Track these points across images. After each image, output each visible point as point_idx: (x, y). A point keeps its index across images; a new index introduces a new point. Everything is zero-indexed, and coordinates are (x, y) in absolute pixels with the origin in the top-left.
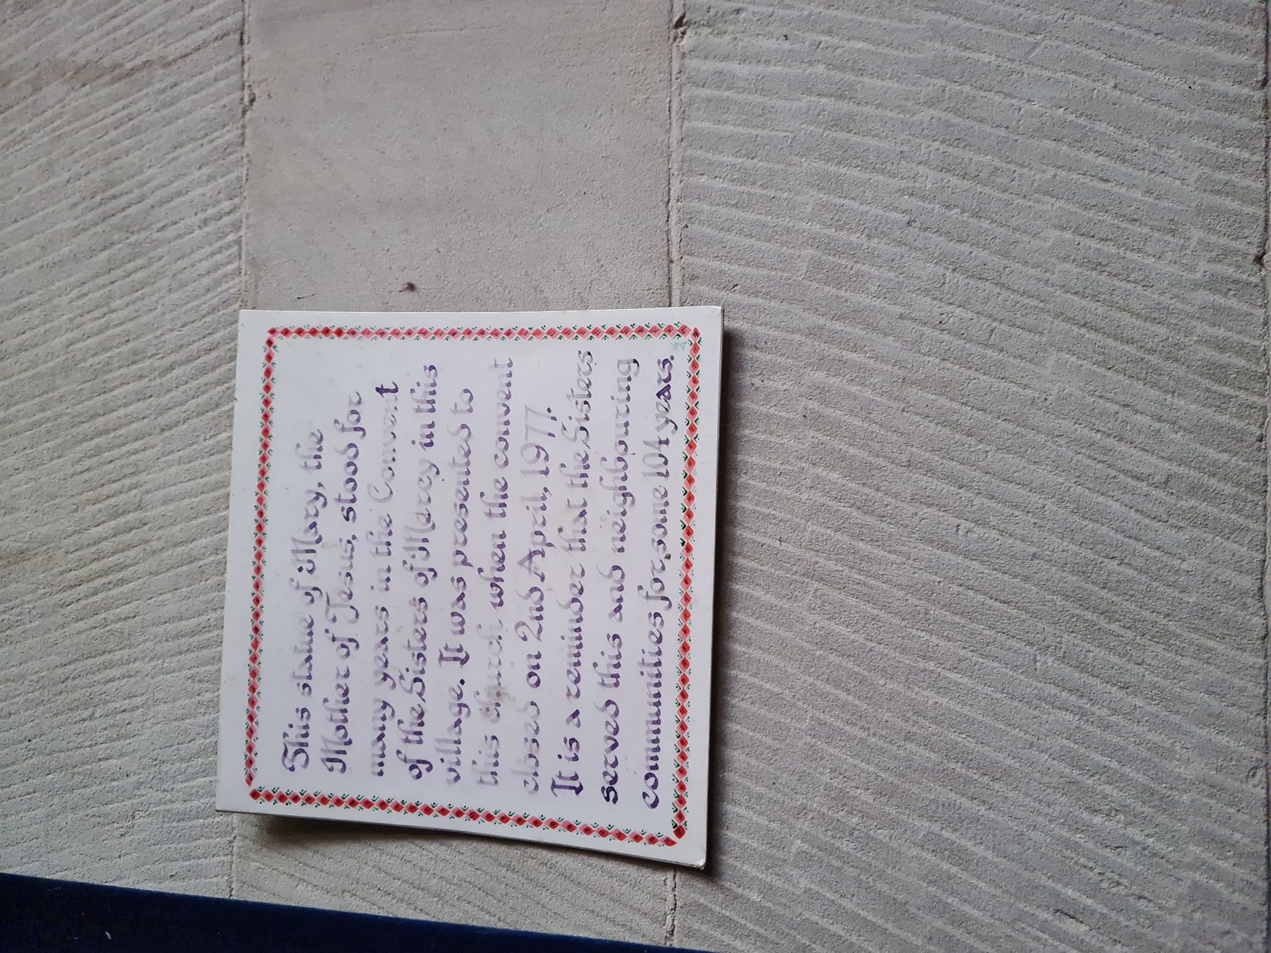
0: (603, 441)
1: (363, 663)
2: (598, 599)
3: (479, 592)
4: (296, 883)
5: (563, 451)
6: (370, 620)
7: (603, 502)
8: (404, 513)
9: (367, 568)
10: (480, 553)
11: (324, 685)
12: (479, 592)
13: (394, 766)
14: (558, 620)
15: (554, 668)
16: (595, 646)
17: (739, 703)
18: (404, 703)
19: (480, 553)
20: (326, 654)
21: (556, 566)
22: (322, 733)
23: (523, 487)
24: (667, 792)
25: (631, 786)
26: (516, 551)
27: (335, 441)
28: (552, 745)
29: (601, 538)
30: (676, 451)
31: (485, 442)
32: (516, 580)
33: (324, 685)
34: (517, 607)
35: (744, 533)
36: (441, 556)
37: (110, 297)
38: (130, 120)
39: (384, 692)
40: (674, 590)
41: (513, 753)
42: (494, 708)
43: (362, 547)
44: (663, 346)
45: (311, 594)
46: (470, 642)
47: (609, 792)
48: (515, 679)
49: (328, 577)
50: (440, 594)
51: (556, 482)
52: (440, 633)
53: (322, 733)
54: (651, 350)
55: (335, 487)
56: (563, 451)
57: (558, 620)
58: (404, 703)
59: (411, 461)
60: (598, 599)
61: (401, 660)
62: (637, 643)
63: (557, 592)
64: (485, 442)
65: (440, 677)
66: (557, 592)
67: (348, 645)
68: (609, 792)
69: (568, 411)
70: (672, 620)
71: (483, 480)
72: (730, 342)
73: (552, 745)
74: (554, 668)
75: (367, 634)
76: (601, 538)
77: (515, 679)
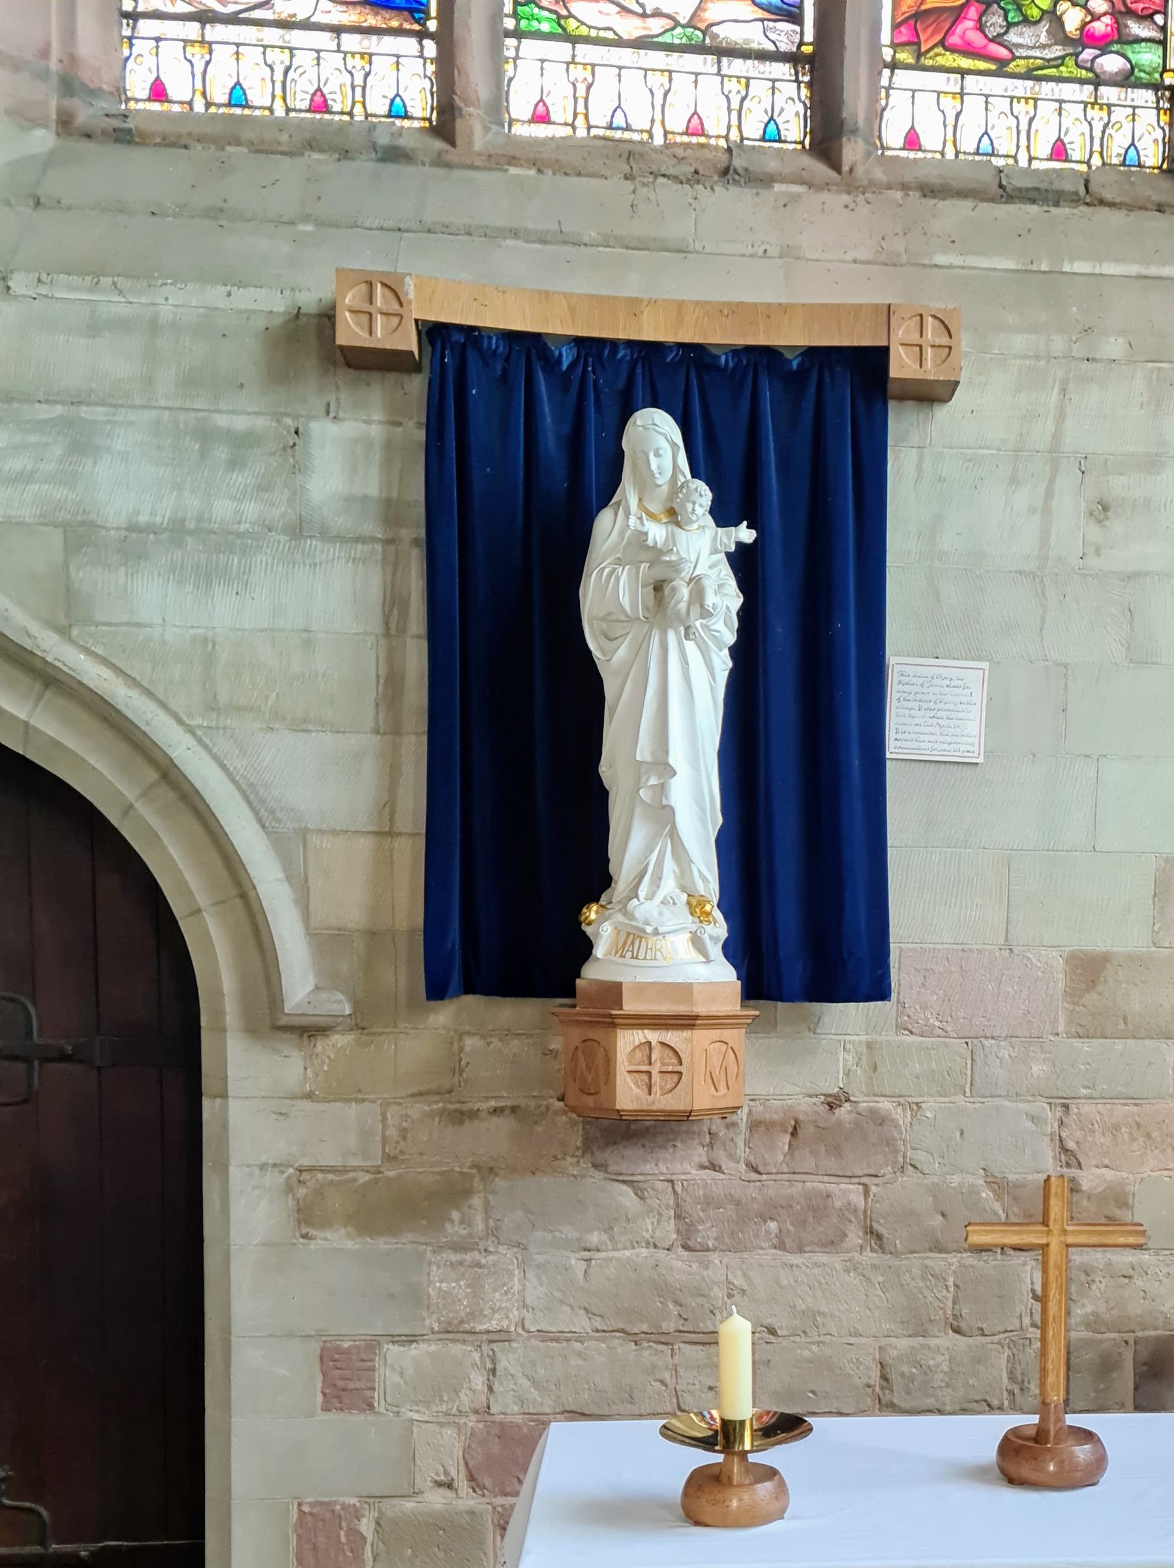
0: (960, 740)
1: (918, 689)
2: (932, 738)
3: (932, 714)
4: (54, 649)
5: (958, 731)
6: (927, 690)
7: (949, 739)
8: (946, 698)
9: (937, 690)
10: (940, 714)
11: (915, 680)
12: (932, 714)
13: (899, 694)
14: (928, 730)
15: (918, 729)
16: (922, 737)
17: (913, 764)
18: (911, 697)
19: (940, 714)
20: (920, 681)
21: (937, 730)
22: (905, 679)
23: (952, 723)
24: (897, 751)
25: (898, 744)
26: (940, 721)
27: (962, 683)
28: (904, 728)
29: (942, 739)
30: (957, 753)
31: (960, 715)
32: (935, 721)
33: (915, 680)
34: (930, 721)
35: (943, 766)
36: (941, 706)
37: (979, 624)
38: (547, 294)
39: (913, 693)
40: (933, 753)
41: (902, 720)
42: (910, 716)
43: (941, 689)
44: (977, 752)
45: (932, 677)
46: (923, 712)
47: (896, 739)
48: (916, 721)
49: (935, 682)
50: (932, 705)
51: (953, 730)
52: (925, 705)
53: (905, 679)
54: (976, 749)
55: (953, 683)
56: (958, 731)
57: (928, 730)
58: (911, 697)
59: (957, 699)
60: (932, 738)
61: (919, 697)
62: (924, 745)
63: (932, 730)
64: (960, 715)
65: (916, 705)
66: (932, 730)
67: (922, 685)
68: (896, 739)
69: (965, 733)
70: (928, 752)
71: (953, 715)
72: (977, 764)
73: (904, 728)
74: (918, 729)
75: (923, 690)
76: (942, 739)
77: (916, 721)
